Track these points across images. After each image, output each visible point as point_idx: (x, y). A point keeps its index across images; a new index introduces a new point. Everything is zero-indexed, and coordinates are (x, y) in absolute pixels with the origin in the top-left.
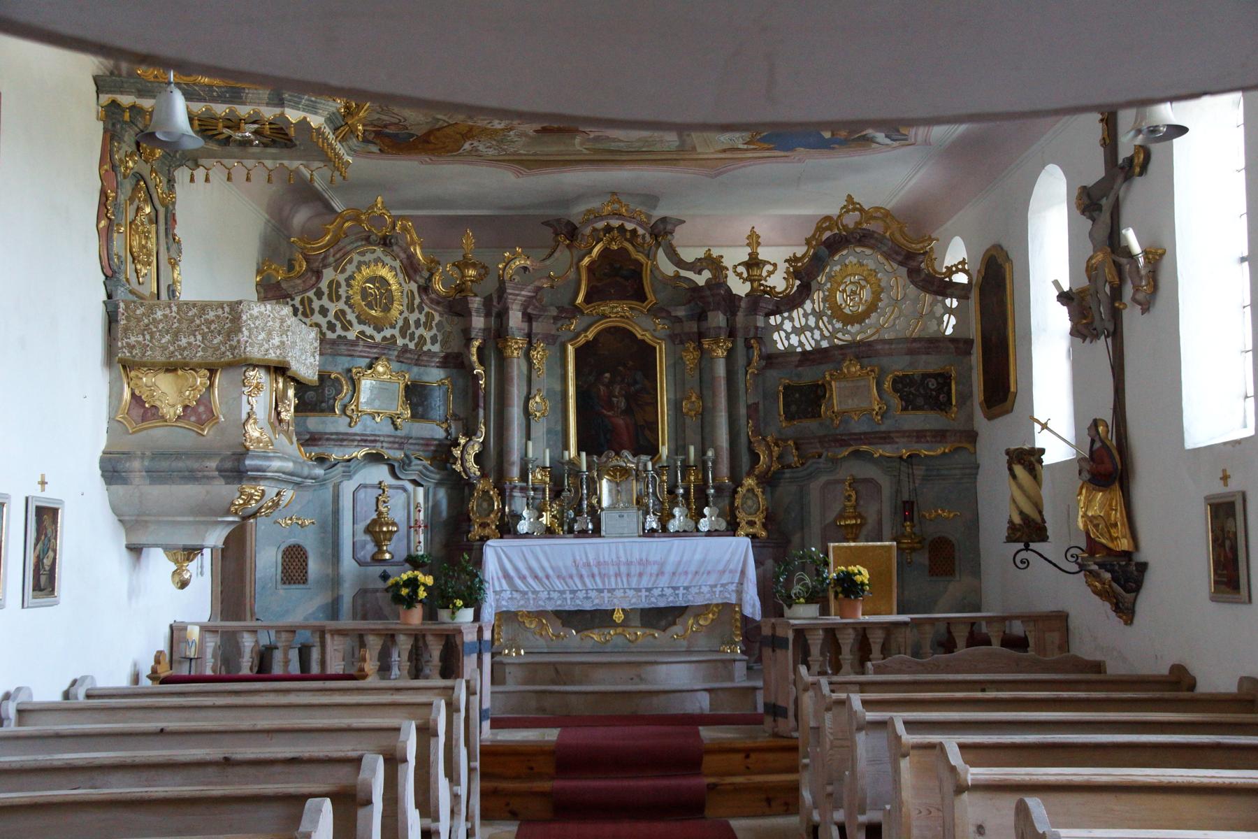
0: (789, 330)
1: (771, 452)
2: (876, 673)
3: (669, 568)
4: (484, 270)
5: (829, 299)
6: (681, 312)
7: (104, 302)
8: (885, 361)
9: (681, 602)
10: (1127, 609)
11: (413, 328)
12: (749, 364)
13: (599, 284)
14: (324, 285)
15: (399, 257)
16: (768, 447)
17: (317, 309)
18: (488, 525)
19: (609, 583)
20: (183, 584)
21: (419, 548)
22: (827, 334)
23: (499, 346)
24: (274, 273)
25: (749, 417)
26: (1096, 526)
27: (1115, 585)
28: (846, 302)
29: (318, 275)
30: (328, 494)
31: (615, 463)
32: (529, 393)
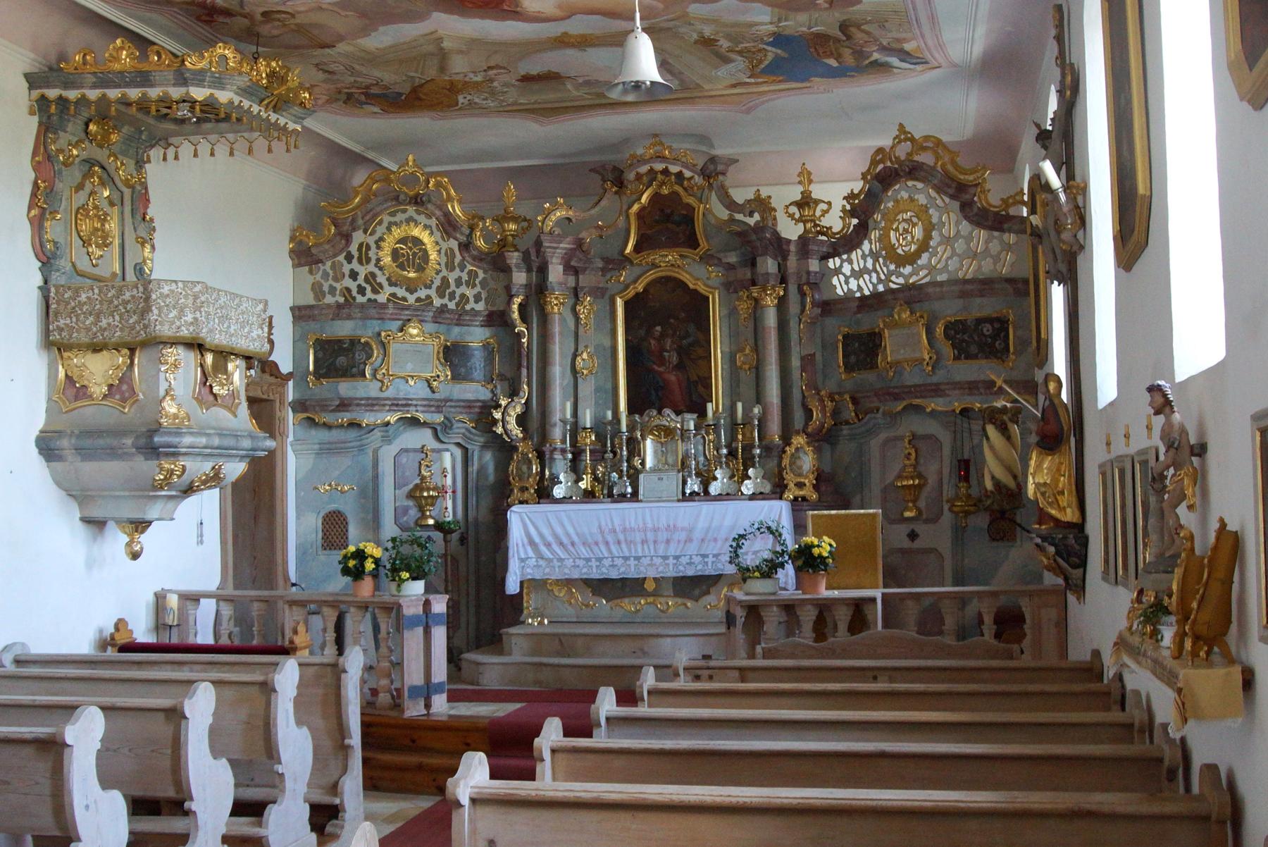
0: (848, 274)
1: (824, 407)
2: (764, 657)
3: (697, 535)
4: (527, 223)
5: (884, 238)
6: (732, 258)
7: (40, 288)
8: (937, 306)
9: (710, 570)
10: (1076, 585)
11: (453, 287)
12: (803, 310)
13: (649, 232)
14: (354, 249)
15: (434, 215)
16: (821, 401)
17: (347, 273)
18: (527, 489)
19: (636, 550)
20: (135, 556)
21: (447, 514)
22: (883, 277)
23: (542, 302)
24: (306, 240)
25: (803, 369)
26: (1043, 494)
27: (1060, 560)
28: (898, 241)
29: (348, 238)
30: (368, 459)
31: (657, 422)
32: (576, 350)
